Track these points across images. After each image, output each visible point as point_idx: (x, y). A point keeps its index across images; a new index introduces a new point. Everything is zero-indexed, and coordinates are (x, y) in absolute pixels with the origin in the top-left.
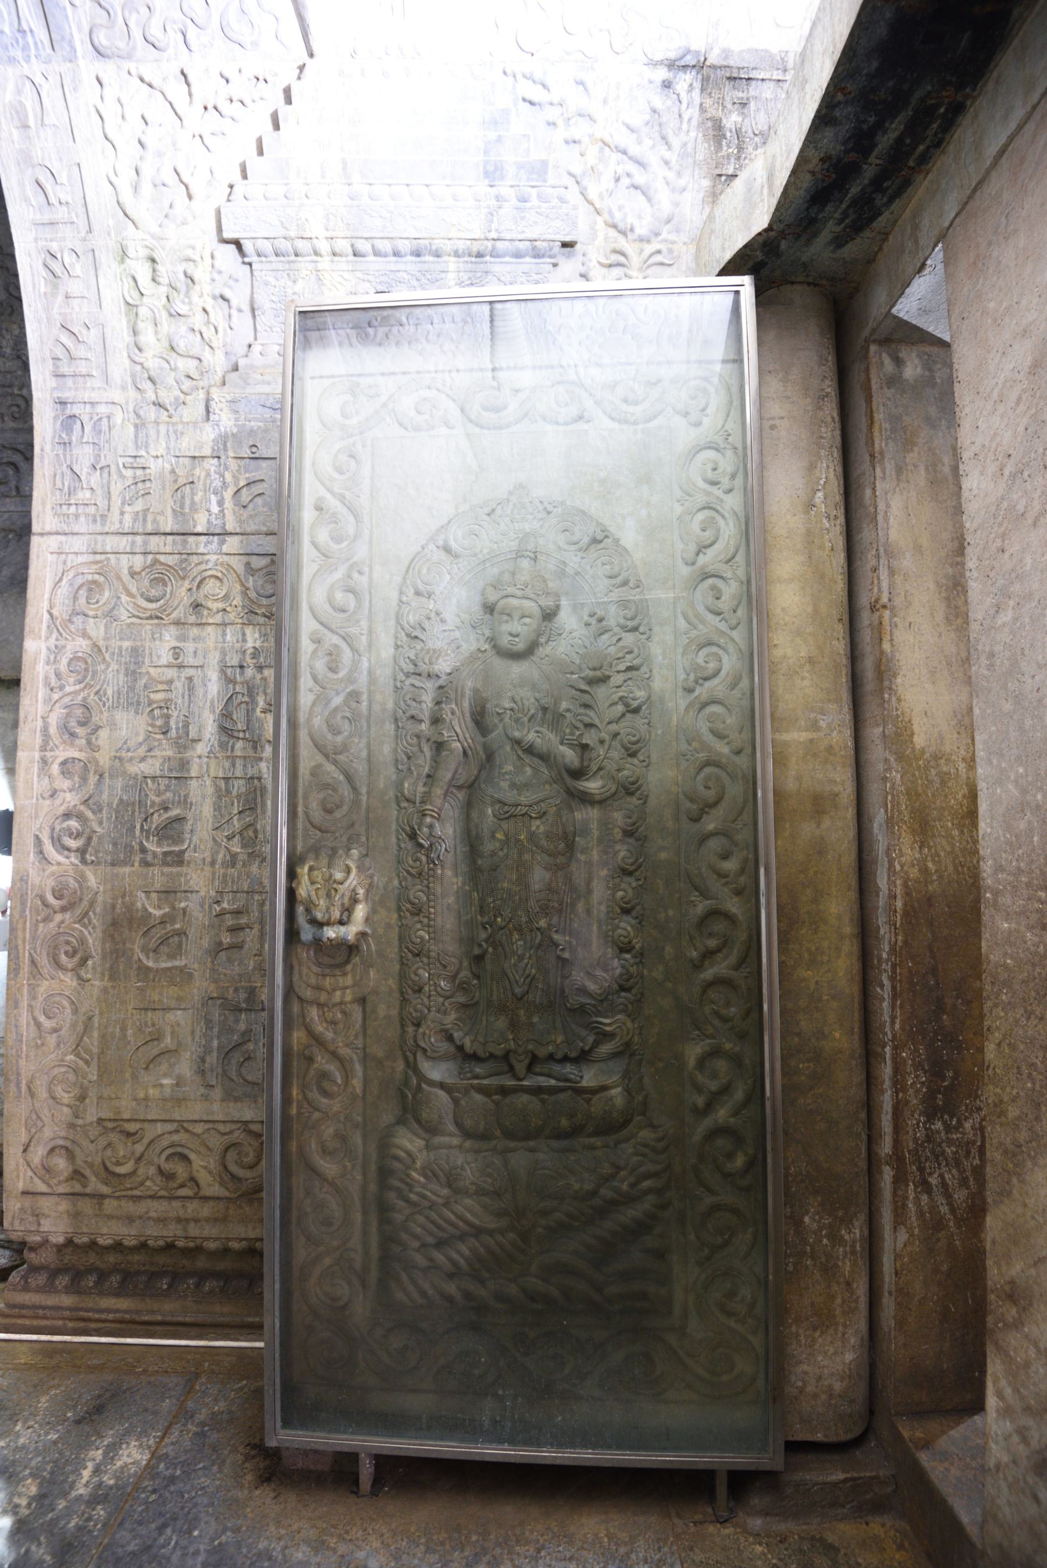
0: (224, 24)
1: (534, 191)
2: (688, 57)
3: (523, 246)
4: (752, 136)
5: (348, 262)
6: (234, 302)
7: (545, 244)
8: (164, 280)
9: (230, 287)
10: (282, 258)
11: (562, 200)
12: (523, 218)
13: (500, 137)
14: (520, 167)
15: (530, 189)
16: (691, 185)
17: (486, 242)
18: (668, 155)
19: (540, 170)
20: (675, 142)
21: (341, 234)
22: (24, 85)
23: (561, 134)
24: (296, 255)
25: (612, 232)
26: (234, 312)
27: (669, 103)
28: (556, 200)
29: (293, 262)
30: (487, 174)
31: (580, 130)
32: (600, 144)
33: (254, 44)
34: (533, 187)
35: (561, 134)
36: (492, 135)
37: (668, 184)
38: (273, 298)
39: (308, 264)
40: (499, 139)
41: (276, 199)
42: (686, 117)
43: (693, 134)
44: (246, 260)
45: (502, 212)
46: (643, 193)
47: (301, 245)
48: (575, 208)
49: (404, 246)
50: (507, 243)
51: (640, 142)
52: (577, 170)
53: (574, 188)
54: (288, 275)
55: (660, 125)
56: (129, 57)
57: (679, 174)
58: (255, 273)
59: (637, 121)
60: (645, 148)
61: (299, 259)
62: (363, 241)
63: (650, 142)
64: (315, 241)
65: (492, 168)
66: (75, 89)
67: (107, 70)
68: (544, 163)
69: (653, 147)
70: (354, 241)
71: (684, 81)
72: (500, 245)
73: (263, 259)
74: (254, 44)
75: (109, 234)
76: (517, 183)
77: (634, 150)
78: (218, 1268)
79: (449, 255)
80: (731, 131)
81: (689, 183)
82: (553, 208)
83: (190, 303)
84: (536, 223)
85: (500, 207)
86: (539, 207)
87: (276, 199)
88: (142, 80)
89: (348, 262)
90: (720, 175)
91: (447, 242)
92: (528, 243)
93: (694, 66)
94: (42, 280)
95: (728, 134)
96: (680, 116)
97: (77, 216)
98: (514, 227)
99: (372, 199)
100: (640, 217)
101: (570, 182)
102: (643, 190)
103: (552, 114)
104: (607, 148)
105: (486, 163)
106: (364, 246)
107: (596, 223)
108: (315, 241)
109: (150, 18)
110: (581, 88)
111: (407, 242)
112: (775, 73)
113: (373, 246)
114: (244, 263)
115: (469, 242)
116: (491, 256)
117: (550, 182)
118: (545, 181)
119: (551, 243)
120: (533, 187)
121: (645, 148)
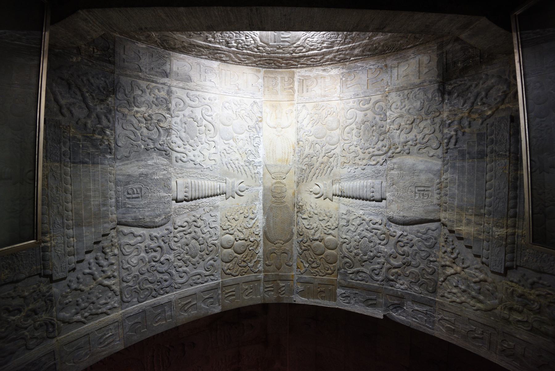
0: (429, 247)
1: (489, 137)
2: (441, 88)
3: (513, 140)
4: (465, 55)
5: (519, 221)
6: (535, 279)
7: (512, 130)
8: (521, 308)
9: (528, 279)
10: (515, 251)
11: (492, 126)
12: (500, 141)
13: (468, 153)
14: (479, 144)
15: (488, 139)
16: (485, 73)
17: (511, 157)
18: (473, 86)
19: (481, 136)
20: (469, 84)
21: (505, 222)
22: (441, 323)
23: (467, 130)
24: (514, 244)
25: (507, 100)
26: (541, 282)
27: (455, 91)
28: (493, 127)
29: (517, 246)
30: (482, 158)
31: (466, 123)
32: (470, 114)
33: (436, 239)
34: (487, 138)
35: (467, 130)
36: (467, 156)
37: (484, 82)
38: (535, 260)
39: (519, 240)
40: (469, 153)
41: (489, 246)
42: (460, 83)
43: (466, 78)
44: (515, 267)
45: (497, 150)
46: (489, 91)
47: (509, 241)
48: (496, 119)
49: (512, 194)
50: (511, 147)
51: (469, 98)
52: (480, 121)
53: (488, 121)
54: (523, 250)
55: (463, 92)
56: (436, 282)
57: (481, 78)
58: (522, 265)
59: (462, 101)
60: (471, 96)
61: (516, 243)
62: (509, 212)
63: (469, 94)
64: (508, 234)
65: (480, 156)
66: (444, 306)
67: (440, 292)
68: (478, 134)
69: (471, 93)
70: (508, 216)
71: (449, 88)
72: (512, 150)
73: (515, 259)
74: (436, 239)
75: (497, 321)
76: (486, 145)
77: (472, 99)
78: (510, 120)
79: (517, 174)
80: (464, 64)
81: (484, 74)
82: (495, 128)
83: (534, 301)
84: (502, 135)
85: (496, 151)
86: (495, 134)
87: (489, 246)
88: (348, 232)
89: (519, 221)
90: (481, 62)
91: (511, 174)
92: (512, 138)
93: (443, 86)
94: (513, 362)
95: (465, 64)
96: (460, 85)
97: (488, 331)
98: (504, 145)
99: (491, 206)
100: (499, 90)
101: (485, 123)
102: (488, 91)
103: (460, 134)
104: (472, 110)
105: (477, 158)
106: (512, 212)
107: (502, 109)
108: (508, 234)
109: (426, 270)
110: (451, 125)
111: (510, 192)
112: (444, 56)
113: (511, 208)
114: (516, 269)
115: (511, 165)
116: (518, 154)
117: (485, 131)
118: (485, 133)
119: (511, 127)
120: (487, 138)
121: (471, 96)
